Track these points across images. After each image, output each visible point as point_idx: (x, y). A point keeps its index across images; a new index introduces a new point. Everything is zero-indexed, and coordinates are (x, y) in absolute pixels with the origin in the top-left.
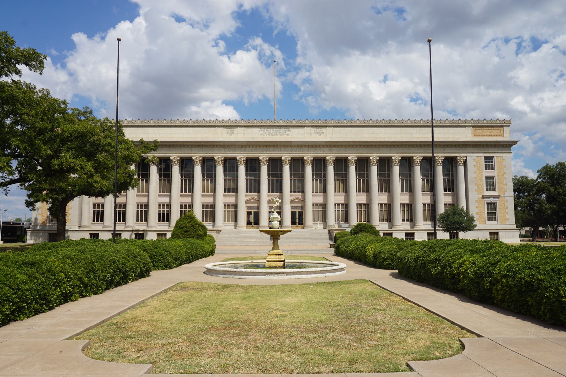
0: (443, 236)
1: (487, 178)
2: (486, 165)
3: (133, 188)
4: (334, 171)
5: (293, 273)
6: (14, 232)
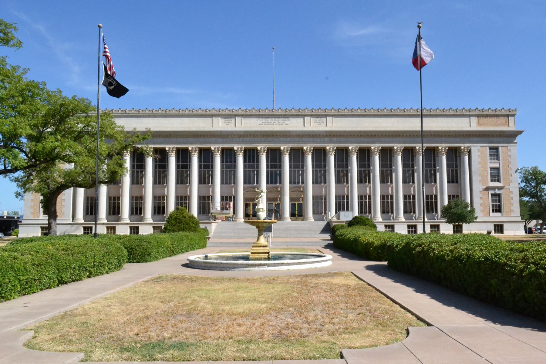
0: (447, 229)
1: (491, 168)
3: (24, 172)
5: (275, 265)
6: (5, 225)
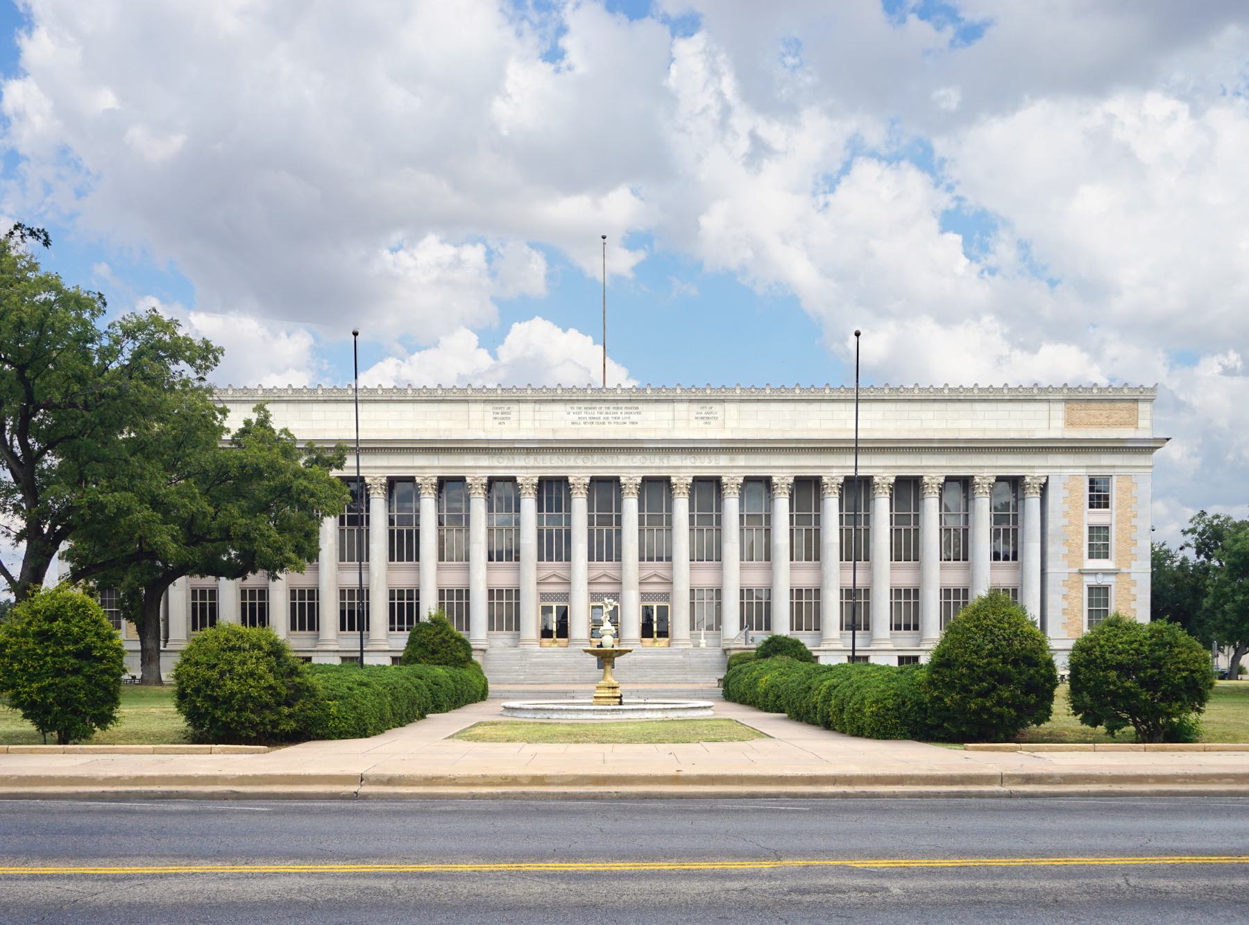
2: (1091, 498)
4: (791, 510)
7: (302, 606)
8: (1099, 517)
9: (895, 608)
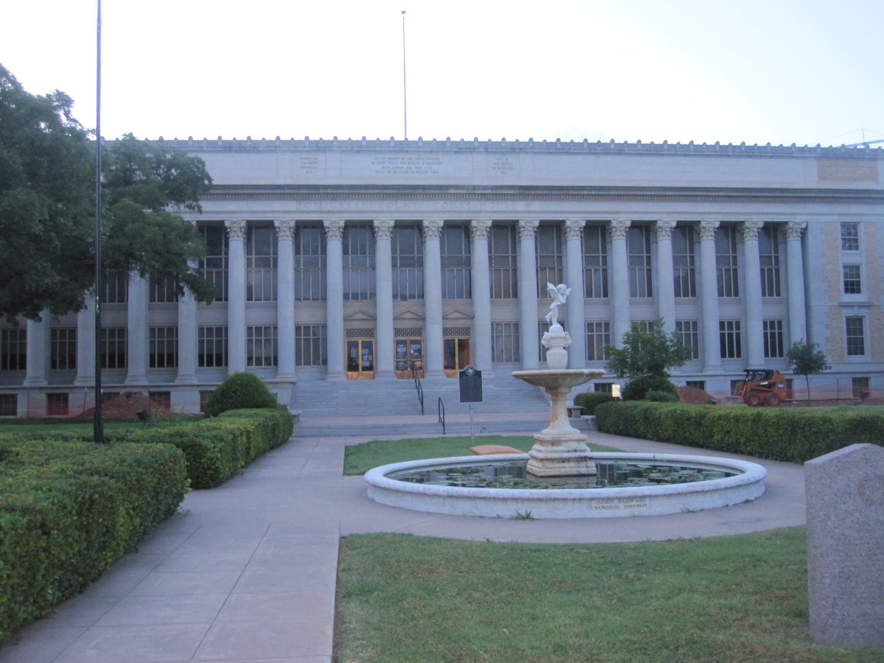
7: (773, 335)
8: (851, 258)
9: (495, 338)
